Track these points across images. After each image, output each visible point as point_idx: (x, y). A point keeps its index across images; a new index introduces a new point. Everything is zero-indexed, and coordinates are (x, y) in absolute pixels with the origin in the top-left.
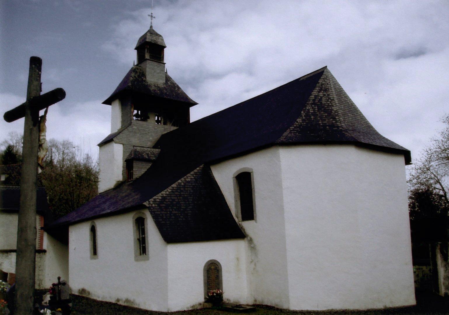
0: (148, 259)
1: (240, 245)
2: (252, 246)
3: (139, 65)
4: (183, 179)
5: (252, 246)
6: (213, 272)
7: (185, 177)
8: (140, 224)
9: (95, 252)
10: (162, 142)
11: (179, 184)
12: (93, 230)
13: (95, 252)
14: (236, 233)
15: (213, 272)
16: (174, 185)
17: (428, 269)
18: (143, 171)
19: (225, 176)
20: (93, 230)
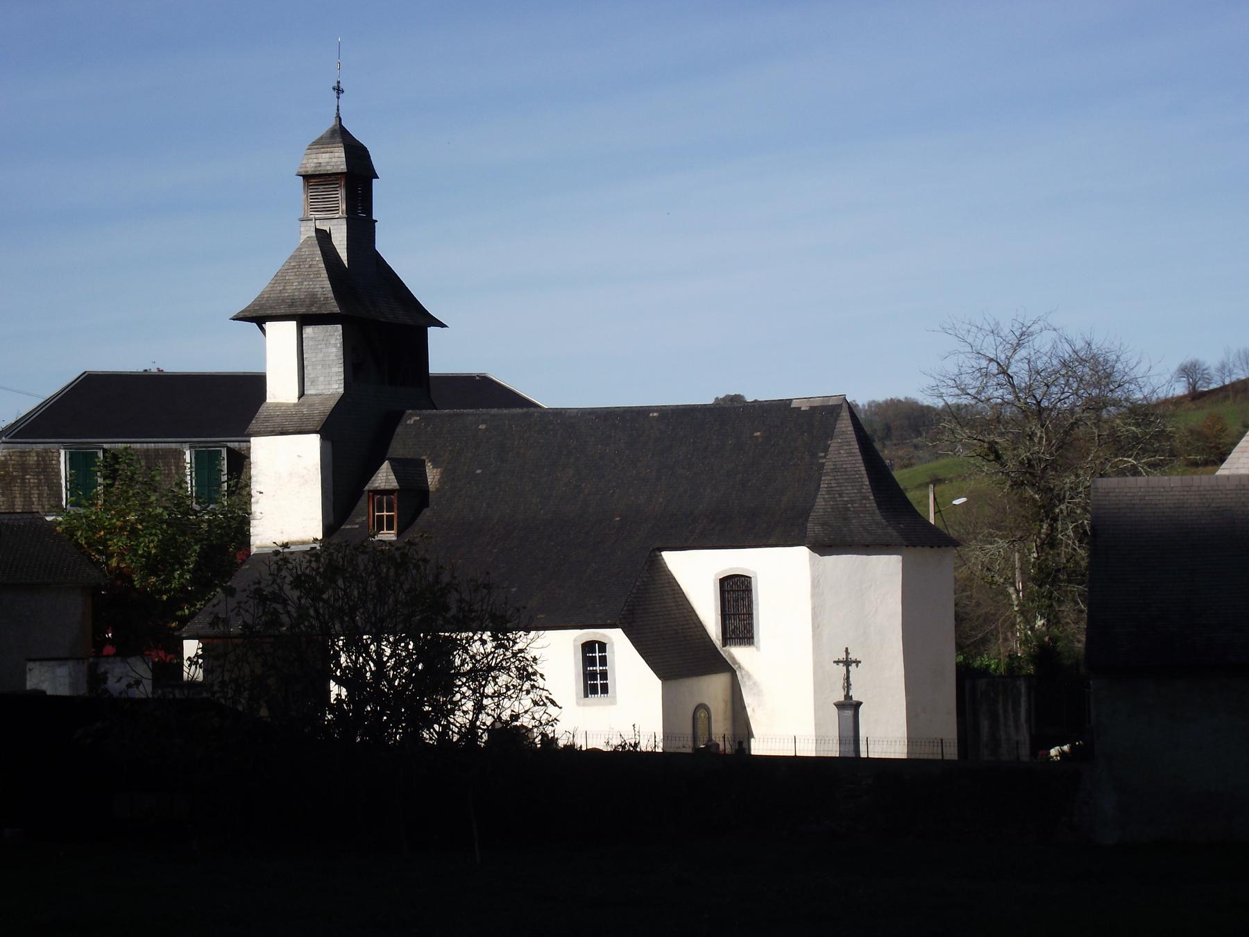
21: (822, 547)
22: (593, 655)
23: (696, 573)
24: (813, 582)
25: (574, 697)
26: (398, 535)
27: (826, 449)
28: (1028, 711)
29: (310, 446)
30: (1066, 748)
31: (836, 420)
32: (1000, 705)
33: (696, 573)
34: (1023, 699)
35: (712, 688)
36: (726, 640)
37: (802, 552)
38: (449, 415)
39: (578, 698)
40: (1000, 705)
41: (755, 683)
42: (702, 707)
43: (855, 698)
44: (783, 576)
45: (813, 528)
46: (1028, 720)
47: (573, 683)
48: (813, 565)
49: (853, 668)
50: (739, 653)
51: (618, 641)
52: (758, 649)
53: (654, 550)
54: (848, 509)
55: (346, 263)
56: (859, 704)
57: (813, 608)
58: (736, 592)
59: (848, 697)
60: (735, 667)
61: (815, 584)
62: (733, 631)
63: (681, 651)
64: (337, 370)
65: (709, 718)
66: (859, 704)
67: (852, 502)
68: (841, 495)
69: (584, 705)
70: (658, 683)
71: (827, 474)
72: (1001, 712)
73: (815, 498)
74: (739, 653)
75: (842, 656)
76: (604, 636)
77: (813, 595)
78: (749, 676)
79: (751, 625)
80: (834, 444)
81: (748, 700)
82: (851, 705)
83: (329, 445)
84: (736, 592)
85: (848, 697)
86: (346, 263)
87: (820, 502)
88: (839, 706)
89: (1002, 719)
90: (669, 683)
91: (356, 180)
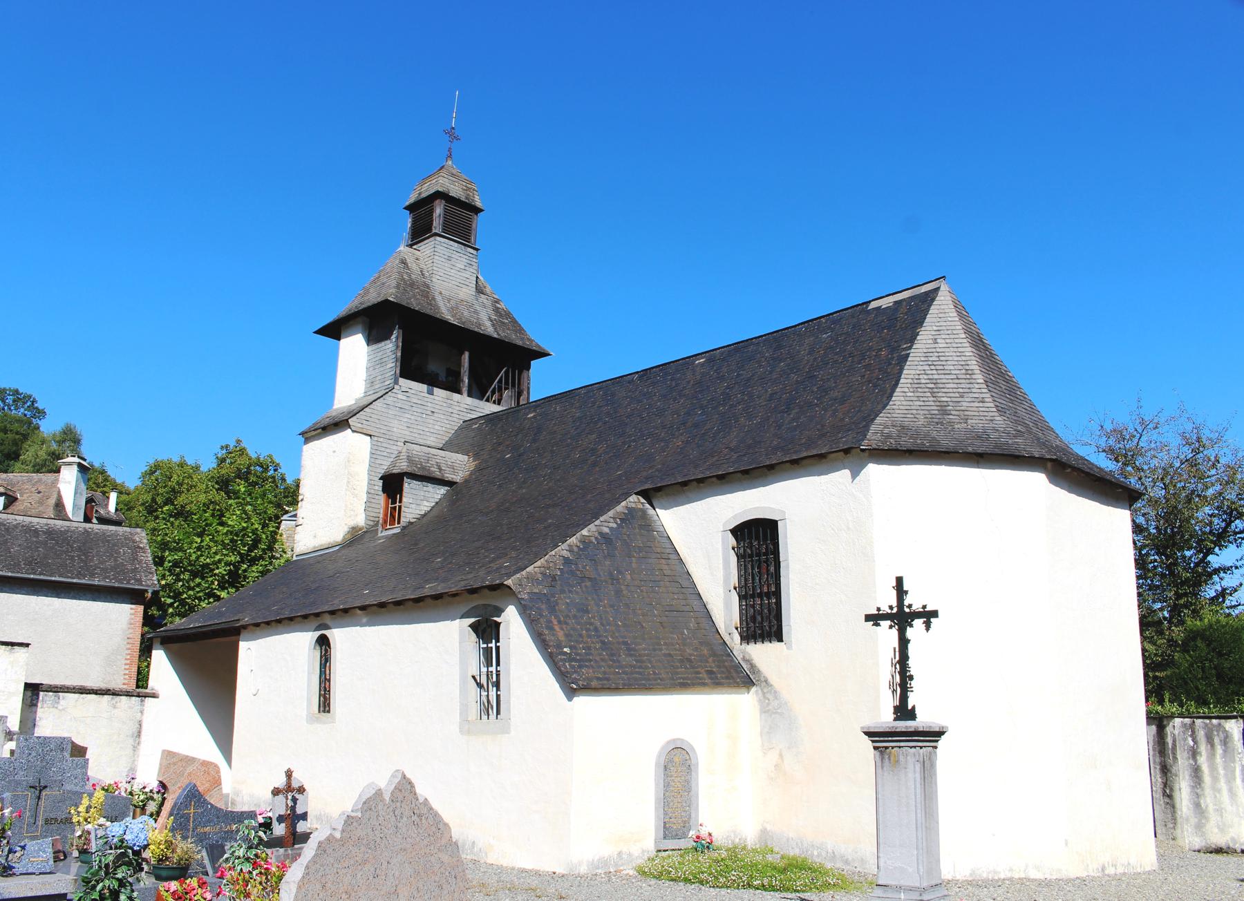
0: (506, 730)
1: (742, 703)
2: (773, 709)
3: (9, 511)
4: (592, 527)
5: (773, 709)
6: (677, 766)
7: (597, 522)
8: (487, 630)
9: (325, 704)
10: (466, 437)
11: (584, 540)
12: (323, 642)
13: (325, 704)
14: (740, 677)
15: (677, 766)
16: (573, 540)
17: (179, 850)
18: (426, 506)
19: (699, 532)
20: (323, 642)
58: (758, 543)
59: (904, 711)
73: (893, 391)
74: (761, 654)
75: (887, 600)
84: (758, 543)
85: (904, 711)
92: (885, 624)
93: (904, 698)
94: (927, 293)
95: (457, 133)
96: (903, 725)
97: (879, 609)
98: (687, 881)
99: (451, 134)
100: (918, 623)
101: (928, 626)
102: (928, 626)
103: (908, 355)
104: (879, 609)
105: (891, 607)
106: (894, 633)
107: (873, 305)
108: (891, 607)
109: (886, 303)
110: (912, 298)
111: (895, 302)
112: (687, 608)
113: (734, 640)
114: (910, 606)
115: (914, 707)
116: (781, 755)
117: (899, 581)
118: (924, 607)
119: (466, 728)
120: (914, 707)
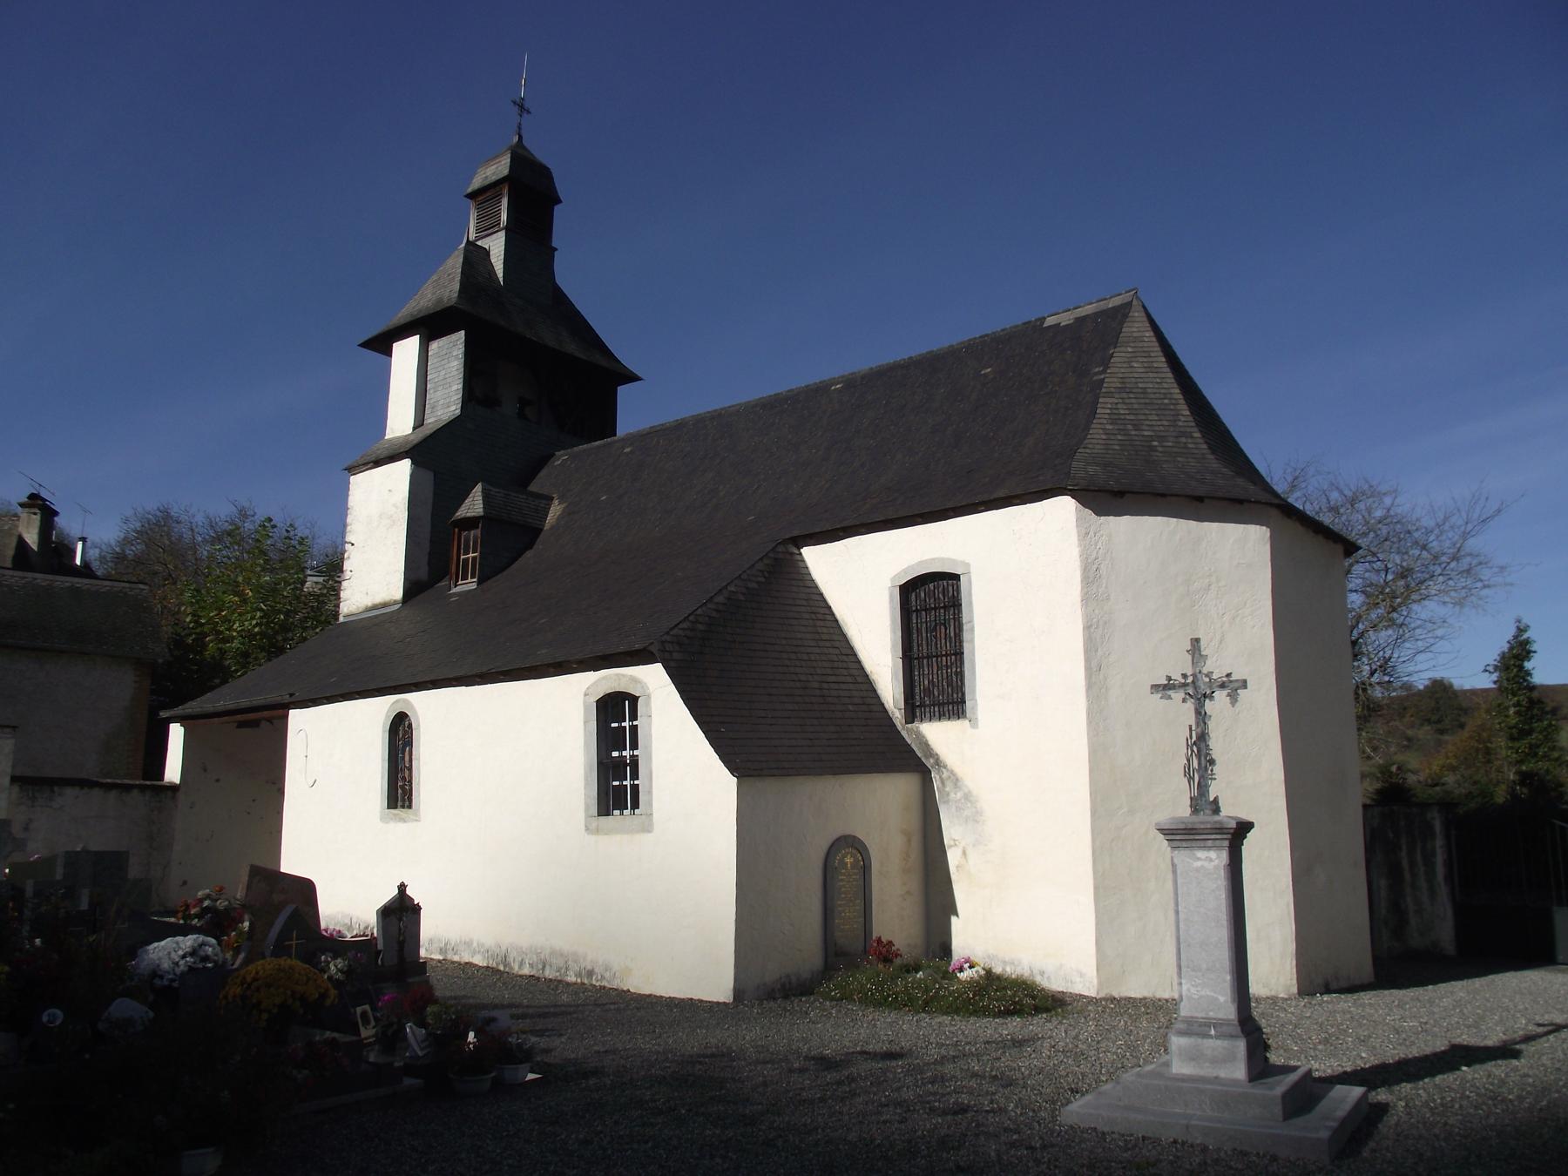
21: (1106, 495)
22: (615, 715)
23: (860, 579)
24: (1085, 569)
25: (581, 815)
26: (479, 583)
27: (1106, 363)
28: (1449, 864)
29: (404, 467)
30: (615, 754)
31: (1121, 323)
32: (1404, 854)
33: (860, 579)
34: (1439, 842)
35: (873, 806)
36: (914, 709)
37: (1063, 507)
38: (598, 447)
39: (588, 816)
40: (1404, 854)
41: (967, 797)
42: (850, 843)
43: (1231, 810)
44: (1024, 562)
45: (1080, 468)
46: (1449, 878)
47: (581, 784)
48: (1084, 535)
49: (1218, 705)
50: (938, 734)
51: (653, 684)
52: (974, 723)
53: (785, 542)
54: (1153, 449)
55: (500, 275)
56: (1181, 835)
57: (1088, 628)
58: (932, 607)
59: (1203, 801)
60: (929, 763)
61: (1091, 575)
62: (928, 692)
63: (803, 724)
64: (456, 387)
65: (866, 870)
66: (1244, 828)
67: (1161, 439)
68: (1137, 427)
69: (597, 831)
70: (729, 782)
71: (1109, 394)
72: (1405, 863)
73: (1087, 428)
74: (938, 734)
75: (1179, 666)
76: (634, 680)
77: (1086, 599)
78: (956, 781)
79: (960, 675)
80: (1119, 356)
81: (952, 830)
82: (1220, 830)
83: (428, 476)
84: (932, 607)
85: (1203, 801)
86: (500, 275)
87: (1096, 435)
88: (1181, 835)
89: (1407, 876)
90: (771, 788)
91: (530, 197)
92: (1178, 696)
93: (1203, 788)
94: (1116, 309)
95: (526, 106)
96: (1206, 818)
97: (1169, 679)
98: (1528, 1039)
99: (521, 107)
100: (1221, 696)
101: (1233, 697)
102: (1233, 697)
103: (1102, 381)
104: (1169, 679)
105: (1185, 676)
106: (1190, 706)
107: (1050, 321)
108: (1185, 676)
109: (1065, 319)
110: (1097, 314)
111: (1077, 319)
112: (849, 679)
113: (897, 715)
114: (1208, 675)
115: (1216, 800)
116: (964, 853)
117: (1196, 642)
118: (1229, 675)
119: (383, 819)
120: (1216, 800)
